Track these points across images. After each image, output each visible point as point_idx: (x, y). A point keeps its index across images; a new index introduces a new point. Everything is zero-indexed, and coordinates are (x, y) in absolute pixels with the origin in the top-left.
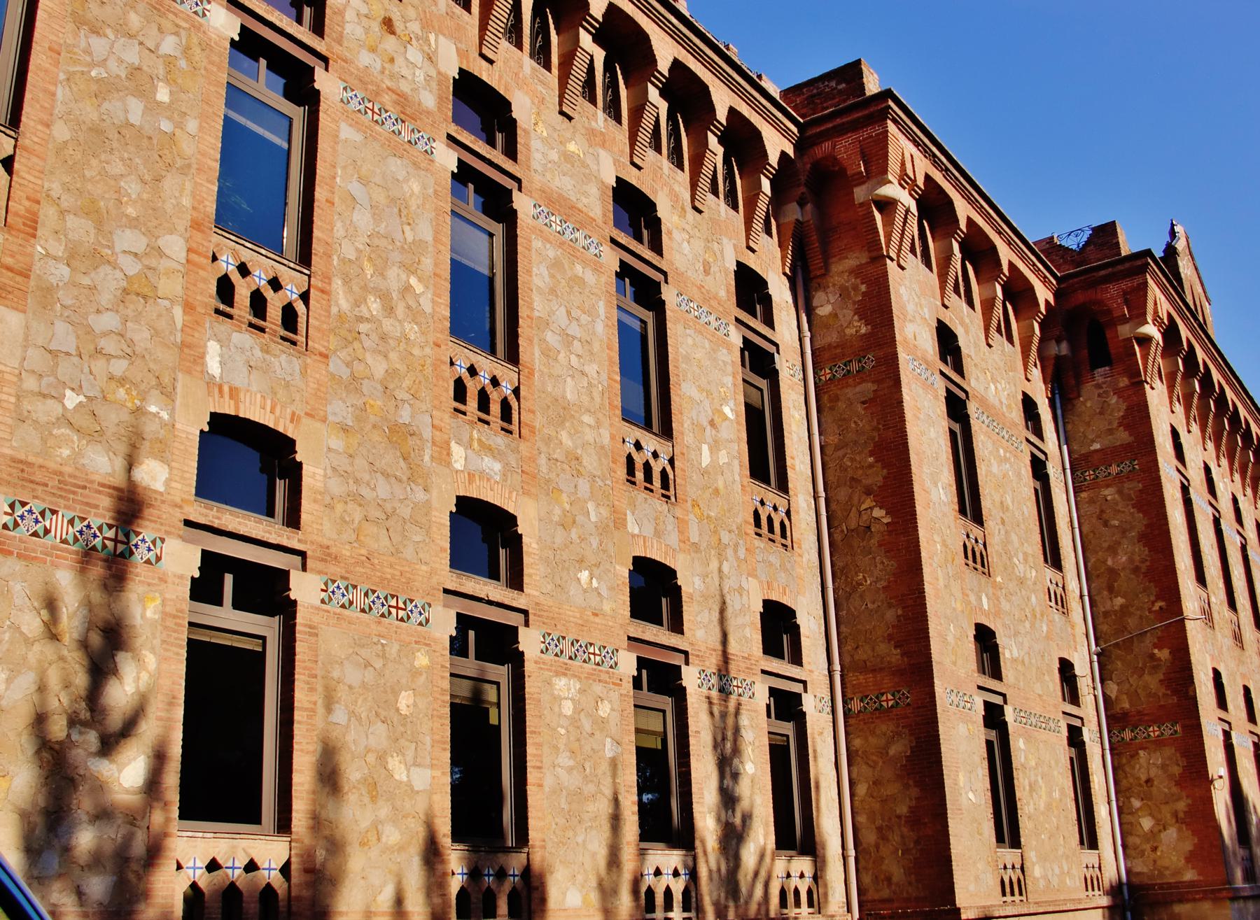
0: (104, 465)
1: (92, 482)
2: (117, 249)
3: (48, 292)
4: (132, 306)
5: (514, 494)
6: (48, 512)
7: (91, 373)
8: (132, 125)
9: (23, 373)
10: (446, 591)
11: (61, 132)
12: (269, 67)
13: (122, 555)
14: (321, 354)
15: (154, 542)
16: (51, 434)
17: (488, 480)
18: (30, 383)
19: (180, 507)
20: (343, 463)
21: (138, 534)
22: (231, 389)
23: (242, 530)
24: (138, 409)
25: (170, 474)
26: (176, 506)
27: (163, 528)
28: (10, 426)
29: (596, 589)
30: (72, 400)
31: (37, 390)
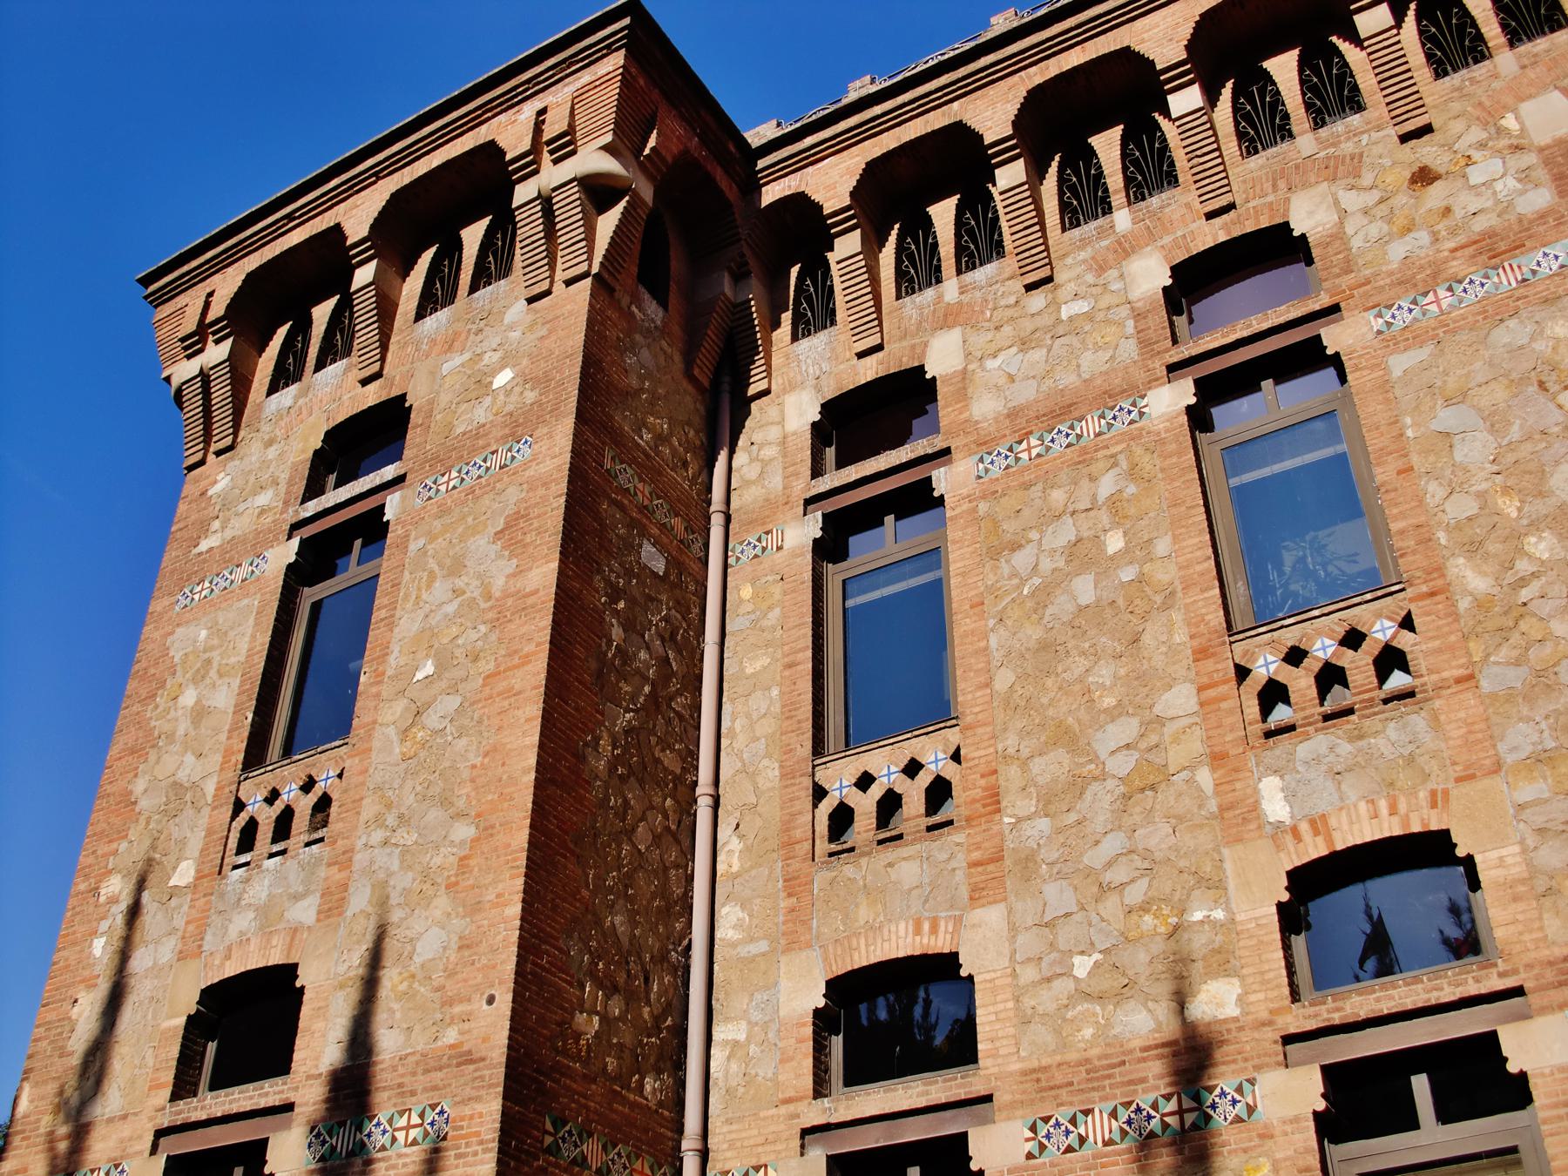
0: (1145, 1022)
1: (1131, 1051)
2: (1103, 755)
3: (1028, 861)
4: (1138, 809)
11: (1004, 679)
13: (1195, 1126)
14: (1458, 681)
16: (1065, 1020)
18: (1028, 974)
19: (1270, 1023)
21: (1210, 1090)
22: (1313, 822)
23: (1386, 1008)
24: (1176, 928)
25: (1243, 985)
26: (1264, 1024)
27: (1249, 1064)
30: (1082, 966)
31: (1038, 977)
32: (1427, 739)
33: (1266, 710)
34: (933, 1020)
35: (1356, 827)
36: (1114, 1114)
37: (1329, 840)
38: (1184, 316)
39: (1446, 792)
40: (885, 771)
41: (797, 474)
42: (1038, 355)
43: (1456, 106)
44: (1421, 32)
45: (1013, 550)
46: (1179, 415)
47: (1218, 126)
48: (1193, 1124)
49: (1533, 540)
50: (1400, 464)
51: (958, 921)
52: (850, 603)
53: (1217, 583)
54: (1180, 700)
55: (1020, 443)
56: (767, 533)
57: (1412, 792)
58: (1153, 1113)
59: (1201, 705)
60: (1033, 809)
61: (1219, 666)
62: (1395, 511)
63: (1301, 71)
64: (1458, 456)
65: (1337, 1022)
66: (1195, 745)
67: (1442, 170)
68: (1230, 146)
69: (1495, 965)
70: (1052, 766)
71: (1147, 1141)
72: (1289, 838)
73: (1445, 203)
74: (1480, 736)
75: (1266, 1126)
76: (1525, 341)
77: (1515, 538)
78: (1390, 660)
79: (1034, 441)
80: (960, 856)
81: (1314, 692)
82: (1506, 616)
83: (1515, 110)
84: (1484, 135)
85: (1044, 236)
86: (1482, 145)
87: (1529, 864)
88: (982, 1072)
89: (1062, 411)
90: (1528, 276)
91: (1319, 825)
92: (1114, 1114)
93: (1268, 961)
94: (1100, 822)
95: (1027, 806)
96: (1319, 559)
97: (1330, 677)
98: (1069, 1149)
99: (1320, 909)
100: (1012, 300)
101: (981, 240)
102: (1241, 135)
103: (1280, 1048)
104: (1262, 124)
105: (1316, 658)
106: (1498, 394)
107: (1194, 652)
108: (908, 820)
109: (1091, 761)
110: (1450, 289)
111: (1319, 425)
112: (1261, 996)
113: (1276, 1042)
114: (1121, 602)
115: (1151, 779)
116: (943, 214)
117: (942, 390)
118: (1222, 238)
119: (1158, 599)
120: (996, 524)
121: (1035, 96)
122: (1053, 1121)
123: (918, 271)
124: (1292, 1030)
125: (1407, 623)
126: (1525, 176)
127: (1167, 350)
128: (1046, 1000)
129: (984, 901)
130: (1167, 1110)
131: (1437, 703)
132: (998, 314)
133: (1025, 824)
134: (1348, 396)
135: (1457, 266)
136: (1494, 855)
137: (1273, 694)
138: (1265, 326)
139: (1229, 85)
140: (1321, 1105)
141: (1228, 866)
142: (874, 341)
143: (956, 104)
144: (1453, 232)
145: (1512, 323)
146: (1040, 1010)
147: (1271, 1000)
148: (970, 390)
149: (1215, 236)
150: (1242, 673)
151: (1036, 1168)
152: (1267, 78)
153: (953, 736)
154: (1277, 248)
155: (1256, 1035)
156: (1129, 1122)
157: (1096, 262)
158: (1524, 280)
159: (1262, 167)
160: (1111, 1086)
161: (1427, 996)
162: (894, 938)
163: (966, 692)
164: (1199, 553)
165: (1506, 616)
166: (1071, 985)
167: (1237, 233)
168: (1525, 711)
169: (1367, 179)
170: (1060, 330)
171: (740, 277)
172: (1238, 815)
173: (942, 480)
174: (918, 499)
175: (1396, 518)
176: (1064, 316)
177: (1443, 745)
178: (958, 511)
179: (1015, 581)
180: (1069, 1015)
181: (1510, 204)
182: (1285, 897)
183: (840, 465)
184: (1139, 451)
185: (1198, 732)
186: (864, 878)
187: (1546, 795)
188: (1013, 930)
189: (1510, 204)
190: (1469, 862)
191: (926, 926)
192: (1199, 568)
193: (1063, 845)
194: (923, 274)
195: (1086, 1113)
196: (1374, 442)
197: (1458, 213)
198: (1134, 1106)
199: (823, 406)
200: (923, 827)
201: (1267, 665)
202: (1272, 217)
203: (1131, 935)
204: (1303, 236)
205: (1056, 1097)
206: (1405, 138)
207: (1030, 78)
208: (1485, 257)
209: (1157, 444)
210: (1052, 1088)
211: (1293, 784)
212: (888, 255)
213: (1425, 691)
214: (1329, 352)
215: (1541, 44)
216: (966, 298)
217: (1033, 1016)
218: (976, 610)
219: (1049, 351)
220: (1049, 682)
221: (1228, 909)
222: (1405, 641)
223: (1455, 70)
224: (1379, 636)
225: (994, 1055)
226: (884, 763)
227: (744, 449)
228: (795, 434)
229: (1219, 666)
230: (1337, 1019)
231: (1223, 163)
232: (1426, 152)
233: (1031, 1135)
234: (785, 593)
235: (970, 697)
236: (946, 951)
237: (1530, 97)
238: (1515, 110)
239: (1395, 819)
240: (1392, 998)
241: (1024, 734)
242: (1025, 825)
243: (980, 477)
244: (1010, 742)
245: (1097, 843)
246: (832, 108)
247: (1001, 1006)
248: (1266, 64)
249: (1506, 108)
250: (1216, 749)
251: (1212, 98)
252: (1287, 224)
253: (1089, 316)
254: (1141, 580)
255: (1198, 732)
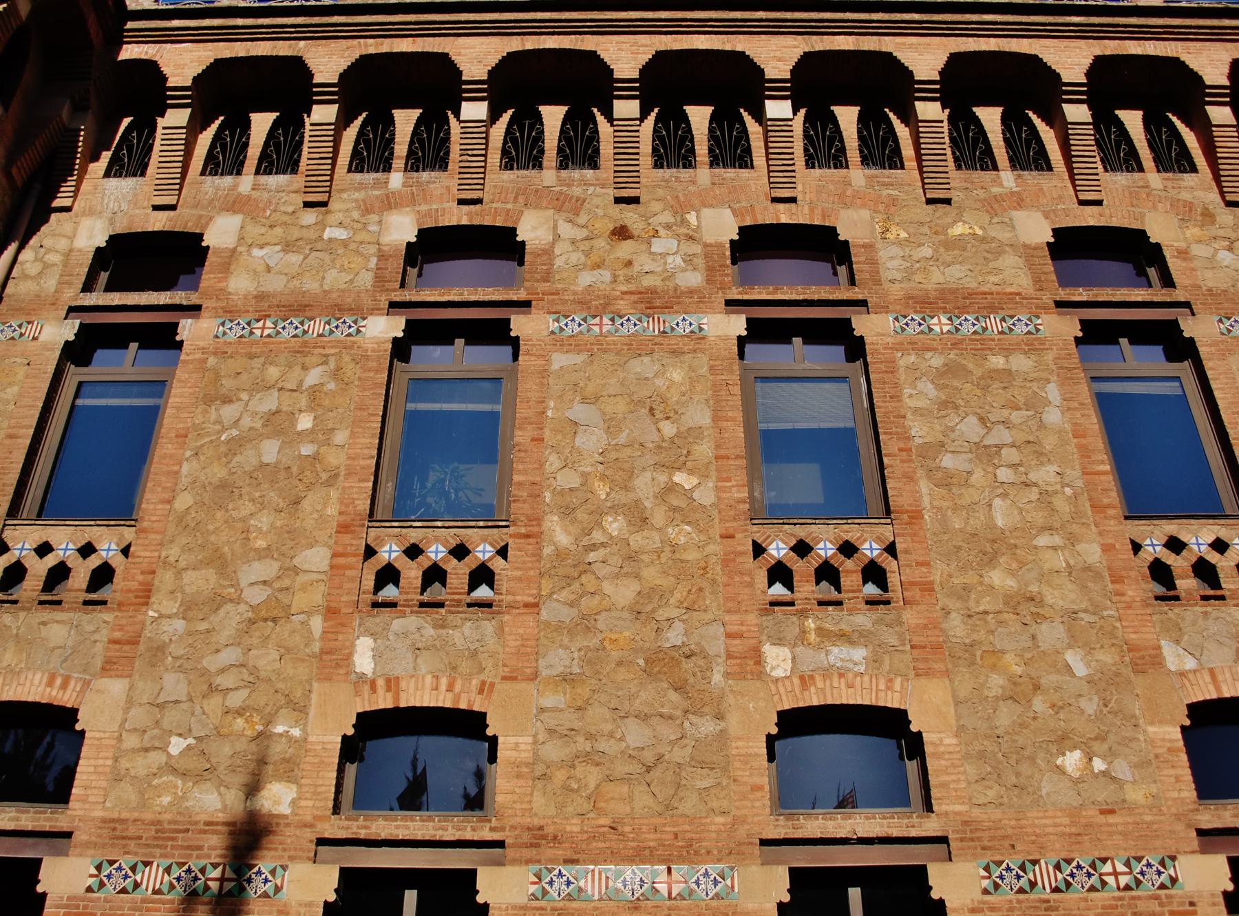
0: (215, 802)
1: (196, 823)
2: (243, 584)
3: (159, 650)
4: (257, 634)
5: (898, 681)
6: (1028, 865)
7: (204, 713)
8: (268, 465)
9: (124, 734)
10: (764, 842)
11: (183, 501)
12: (1131, 343)
13: (230, 893)
14: (526, 605)
15: (1162, 863)
16: (150, 785)
17: (841, 675)
18: (131, 741)
19: (311, 826)
20: (569, 719)
21: (251, 867)
22: (388, 681)
23: (401, 834)
24: (260, 734)
25: (299, 792)
26: (305, 826)
27: (286, 854)
28: (105, 789)
29: (1104, 773)
30: (177, 745)
31: (139, 746)
32: (491, 642)
33: (379, 585)
34: (49, 761)
35: (419, 693)
36: (168, 870)
37: (397, 697)
38: (416, 270)
39: (492, 685)
40: (63, 546)
41: (70, 284)
42: (295, 258)
43: (661, 192)
44: (655, 131)
45: (224, 402)
46: (386, 342)
47: (491, 138)
48: (229, 891)
49: (610, 519)
50: (535, 434)
51: (86, 684)
52: (79, 402)
53: (372, 478)
54: (316, 559)
55: (258, 321)
56: (29, 323)
57: (468, 678)
58: (200, 876)
59: (332, 567)
60: (175, 611)
61: (354, 542)
62: (520, 467)
63: (564, 124)
64: (578, 441)
65: (362, 837)
66: (317, 597)
67: (636, 233)
68: (495, 157)
69: (490, 821)
70: (200, 581)
71: (192, 896)
72: (367, 688)
73: (629, 257)
74: (529, 650)
75: (285, 905)
76: (651, 375)
77: (598, 514)
78: (482, 575)
79: (269, 324)
80: (105, 632)
81: (419, 582)
82: (574, 568)
83: (698, 212)
84: (673, 220)
85: (333, 170)
86: (668, 227)
87: (535, 753)
88: (69, 812)
89: (299, 308)
90: (668, 330)
91: (392, 684)
92: (168, 870)
93: (323, 778)
94: (224, 636)
95: (171, 607)
96: (454, 485)
97: (435, 575)
98: (124, 891)
99: (373, 747)
100: (290, 209)
101: (282, 155)
102: (505, 152)
103: (313, 846)
104: (523, 150)
105: (429, 558)
106: (621, 406)
107: (338, 526)
108: (70, 590)
109: (232, 586)
110: (612, 320)
111: (486, 385)
112: (310, 803)
113: (311, 841)
114: (295, 470)
115: (275, 613)
116: (261, 123)
117: (211, 259)
118: (465, 222)
119: (324, 476)
120: (218, 377)
121: (364, 62)
122: (116, 865)
123: (225, 159)
124: (327, 836)
125: (503, 552)
126: (689, 259)
127: (394, 290)
128: (141, 765)
129: (113, 673)
130: (211, 876)
131: (506, 618)
132: (276, 216)
133: (164, 620)
134: (514, 373)
135: (622, 305)
136: (512, 740)
137: (388, 575)
138: (473, 298)
139: (510, 112)
140: (332, 897)
141: (314, 696)
142: (171, 200)
143: (302, 43)
144: (628, 280)
145: (646, 359)
146: (133, 773)
147: (317, 808)
148: (232, 267)
149: (460, 219)
150: (370, 552)
151: (90, 900)
152: (539, 118)
153: (128, 534)
154: (501, 244)
155: (298, 832)
156: (179, 879)
157: (365, 205)
158: (664, 332)
159: (511, 181)
160: (173, 847)
161: (433, 832)
162: (28, 684)
163: (150, 502)
164: (366, 451)
165: (574, 568)
166: (164, 759)
167: (477, 222)
168: (566, 641)
169: (582, 219)
170: (319, 246)
171: (79, 108)
172: (333, 660)
173: (187, 329)
174: (161, 337)
175: (519, 472)
176: (326, 236)
177: (501, 650)
178: (190, 358)
179: (218, 427)
180: (155, 782)
181: (673, 274)
182: (350, 732)
183: (109, 288)
184: (347, 358)
185: (322, 587)
186: (18, 628)
187: (562, 706)
188: (130, 702)
189: (673, 274)
190: (493, 741)
191: (58, 681)
192: (362, 462)
193: (190, 645)
194: (229, 162)
195: (146, 864)
196: (522, 411)
197: (636, 268)
198: (186, 867)
199: (111, 236)
200: (81, 600)
201: (390, 551)
202: (506, 220)
203: (223, 731)
204: (523, 242)
205: (124, 846)
206: (618, 200)
207: (366, 46)
208: (643, 306)
209: (362, 358)
210: (124, 838)
211: (382, 648)
212: (205, 139)
213: (500, 606)
214: (513, 334)
215: (730, 173)
216: (255, 194)
217: (125, 776)
218: (180, 440)
219: (305, 259)
220: (219, 514)
221: (304, 730)
222: (498, 564)
223: (668, 167)
224: (480, 555)
225: (84, 800)
226: (65, 540)
227: (33, 248)
228: (80, 251)
229: (354, 542)
230: (363, 834)
231: (485, 167)
232: (629, 216)
233: (96, 872)
234: (27, 377)
235: (151, 507)
236: (69, 705)
237: (711, 206)
238: (698, 212)
239: (449, 695)
240: (407, 828)
241: (186, 549)
242: (164, 621)
243: (217, 337)
244: (173, 552)
245: (218, 651)
246: (204, 5)
247: (101, 762)
248: (541, 108)
249: (693, 208)
250: (333, 605)
251: (494, 116)
252: (515, 229)
253: (345, 243)
254: (315, 457)
255: (322, 587)
